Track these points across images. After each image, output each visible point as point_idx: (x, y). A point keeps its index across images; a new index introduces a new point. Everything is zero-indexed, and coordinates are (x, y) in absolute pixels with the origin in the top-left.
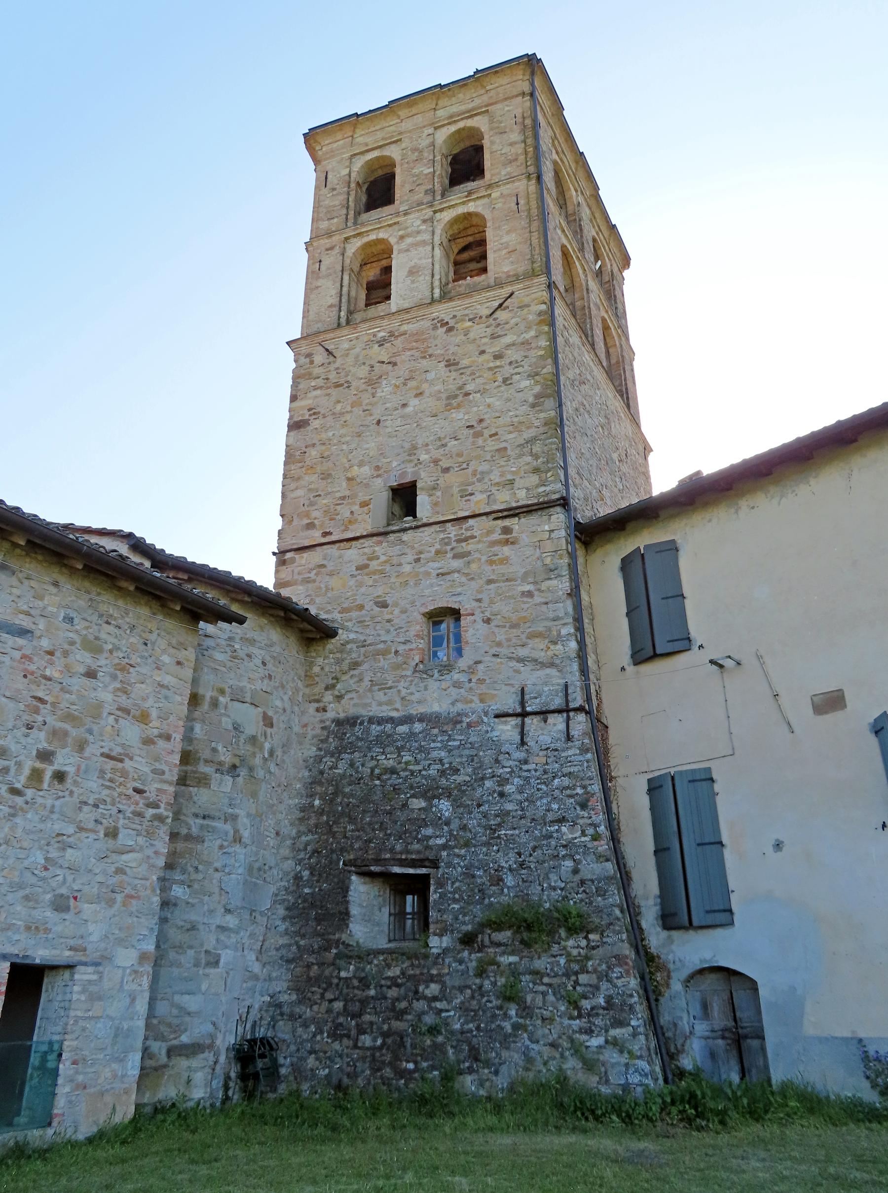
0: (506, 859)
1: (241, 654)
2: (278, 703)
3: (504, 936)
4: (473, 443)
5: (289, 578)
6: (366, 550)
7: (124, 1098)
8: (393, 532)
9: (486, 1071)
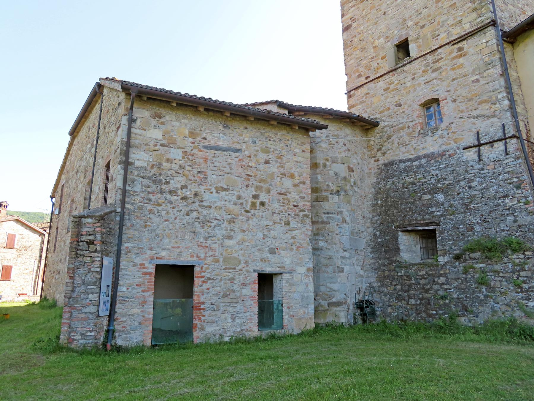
0: (475, 218)
1: (333, 142)
2: (355, 161)
3: (477, 255)
4: (436, 7)
5: (354, 103)
6: (387, 80)
7: (310, 321)
8: (399, 68)
9: (472, 316)
